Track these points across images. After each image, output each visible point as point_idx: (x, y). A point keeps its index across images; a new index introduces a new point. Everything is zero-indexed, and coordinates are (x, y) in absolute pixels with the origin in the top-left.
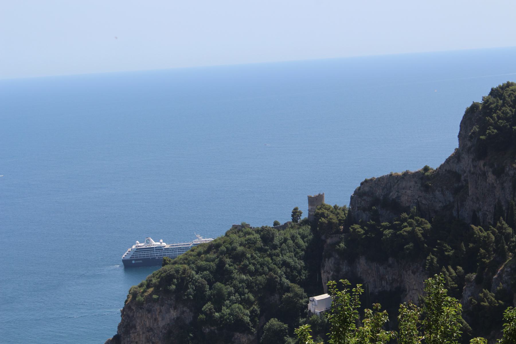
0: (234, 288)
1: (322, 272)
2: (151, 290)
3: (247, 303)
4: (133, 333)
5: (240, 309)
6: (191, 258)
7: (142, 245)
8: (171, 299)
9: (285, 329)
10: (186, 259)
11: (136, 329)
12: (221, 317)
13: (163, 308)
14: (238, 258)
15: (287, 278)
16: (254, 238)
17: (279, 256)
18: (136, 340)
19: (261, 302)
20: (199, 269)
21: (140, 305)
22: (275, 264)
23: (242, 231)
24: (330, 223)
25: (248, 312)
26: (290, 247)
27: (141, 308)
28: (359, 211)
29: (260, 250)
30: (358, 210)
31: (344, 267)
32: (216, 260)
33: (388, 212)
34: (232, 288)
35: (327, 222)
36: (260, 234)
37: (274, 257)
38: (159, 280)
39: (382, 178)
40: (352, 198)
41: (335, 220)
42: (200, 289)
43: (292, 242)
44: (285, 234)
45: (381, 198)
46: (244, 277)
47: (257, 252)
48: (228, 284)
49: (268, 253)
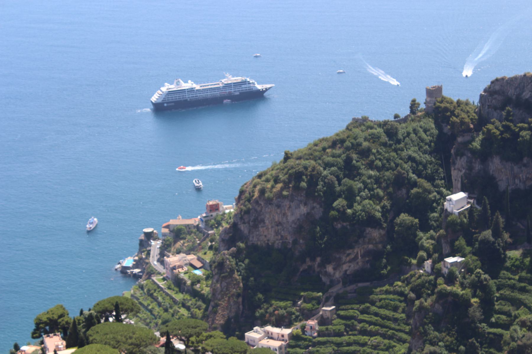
0: (363, 184)
1: (453, 169)
2: (279, 186)
3: (376, 198)
4: (262, 227)
5: (371, 205)
6: (317, 154)
7: (173, 87)
8: (301, 196)
9: (416, 224)
10: (312, 155)
11: (264, 223)
12: (353, 214)
13: (293, 204)
14: (365, 153)
15: (413, 173)
16: (378, 133)
17: (403, 150)
18: (265, 234)
19: (390, 196)
20: (327, 165)
21: (269, 201)
22: (401, 159)
23: (364, 125)
24: (462, 123)
25: (378, 207)
26: (413, 141)
27: (270, 204)
28: (490, 110)
29: (385, 145)
30: (488, 108)
31: (477, 165)
32: (343, 156)
33: (521, 111)
34: (361, 184)
35: (459, 121)
36: (383, 128)
37: (399, 152)
38: (287, 176)
39: (515, 78)
40: (481, 96)
41: (467, 120)
42: (330, 186)
43: (414, 135)
44: (407, 128)
45: (514, 97)
46: (372, 173)
47: (382, 147)
48: (357, 181)
49: (393, 147)
